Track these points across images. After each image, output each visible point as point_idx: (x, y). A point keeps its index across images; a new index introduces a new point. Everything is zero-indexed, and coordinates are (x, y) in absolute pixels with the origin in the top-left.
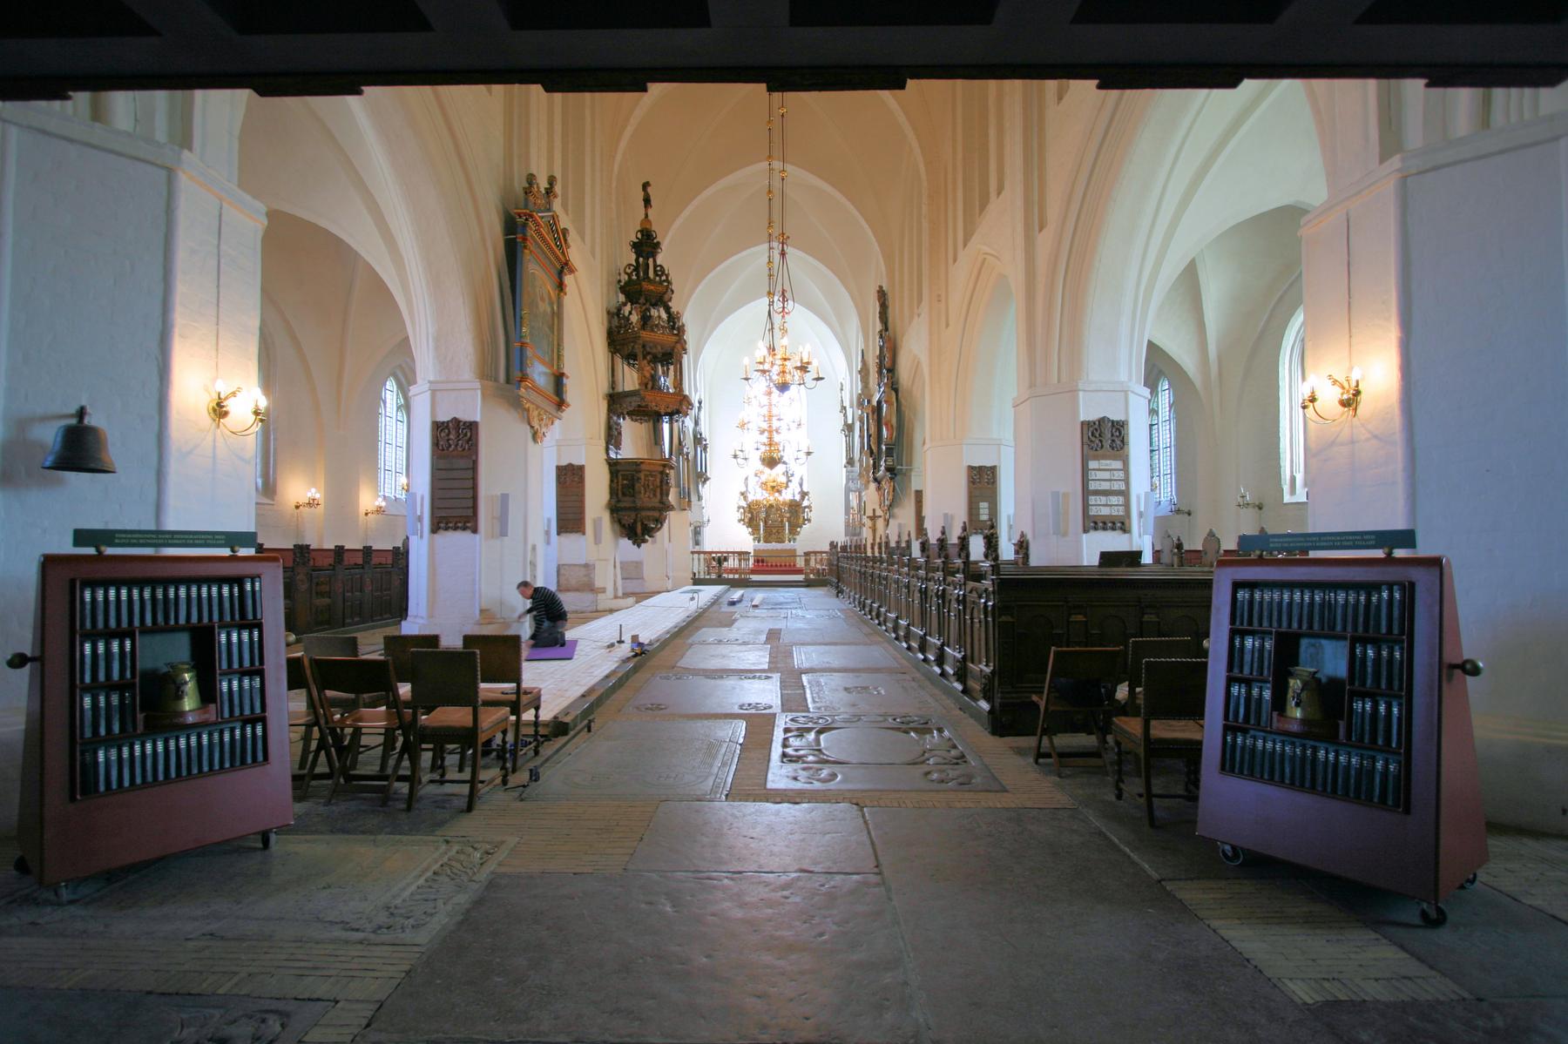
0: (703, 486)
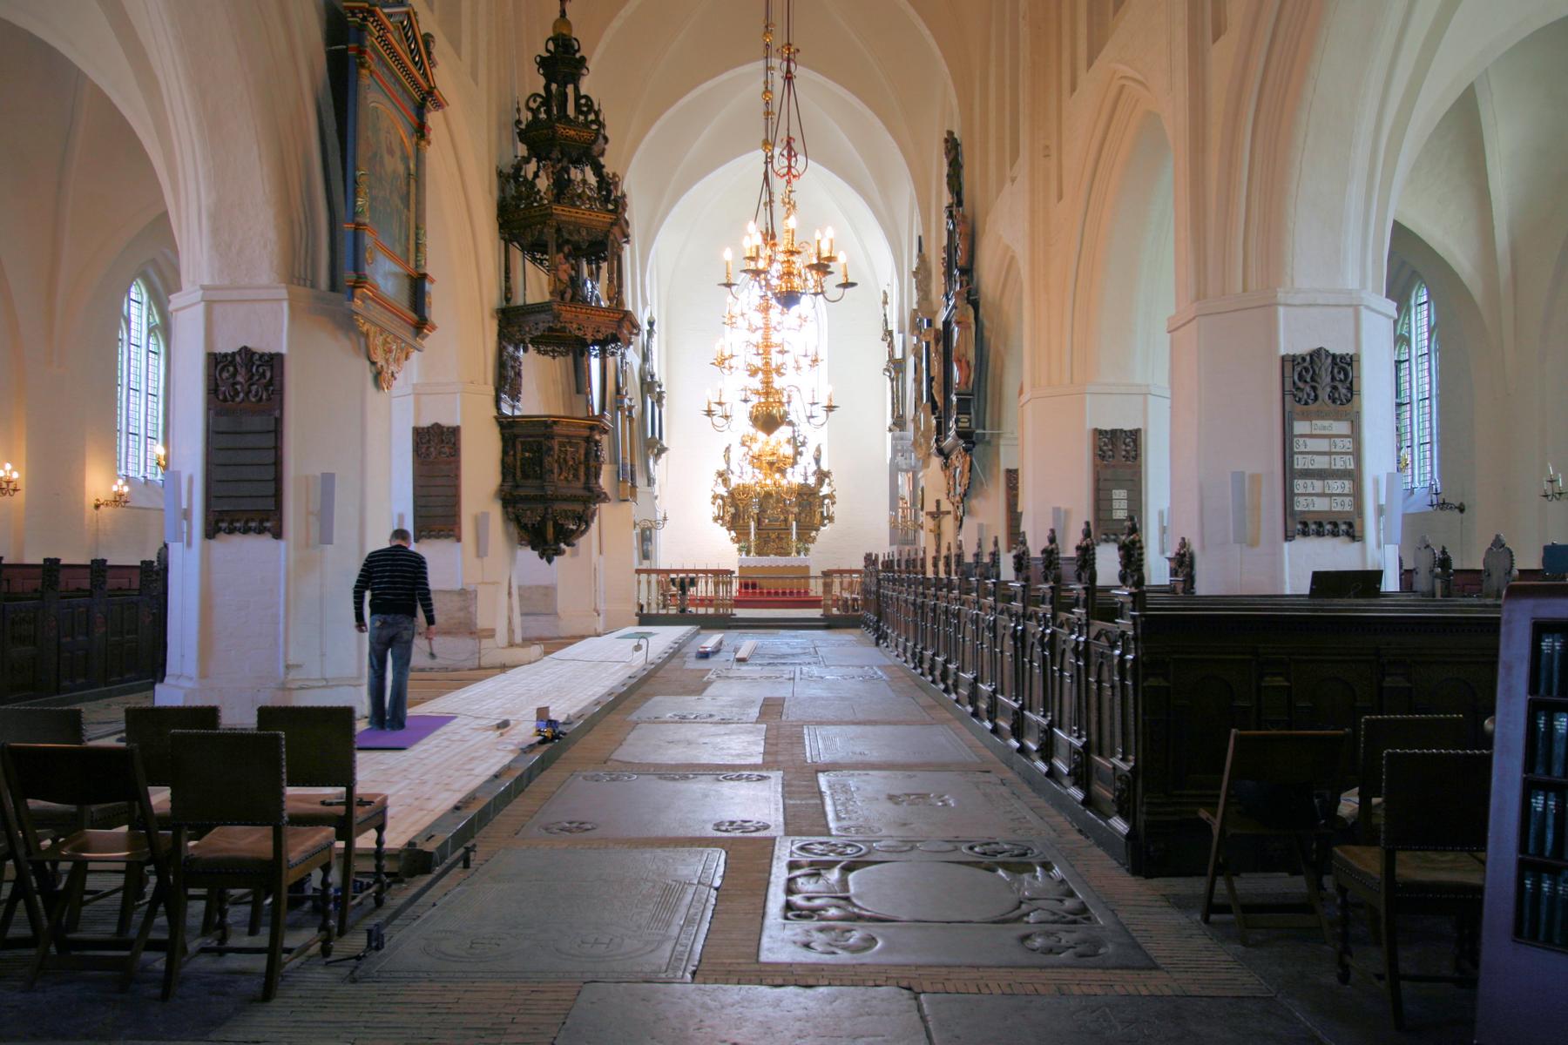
0: (655, 462)
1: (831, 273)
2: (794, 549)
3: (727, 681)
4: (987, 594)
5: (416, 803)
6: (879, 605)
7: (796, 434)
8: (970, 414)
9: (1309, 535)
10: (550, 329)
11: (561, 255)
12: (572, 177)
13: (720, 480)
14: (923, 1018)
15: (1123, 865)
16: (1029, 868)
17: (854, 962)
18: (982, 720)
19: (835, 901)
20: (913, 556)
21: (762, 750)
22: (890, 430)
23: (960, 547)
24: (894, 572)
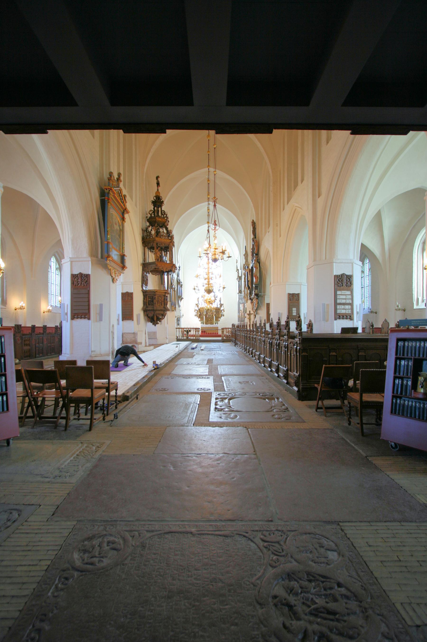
0: (181, 301)
6: (235, 337)
10: (155, 268)
11: (158, 250)
12: (160, 230)
14: (249, 434)
18: (261, 364)
19: (227, 407)
21: (208, 371)
23: (256, 322)
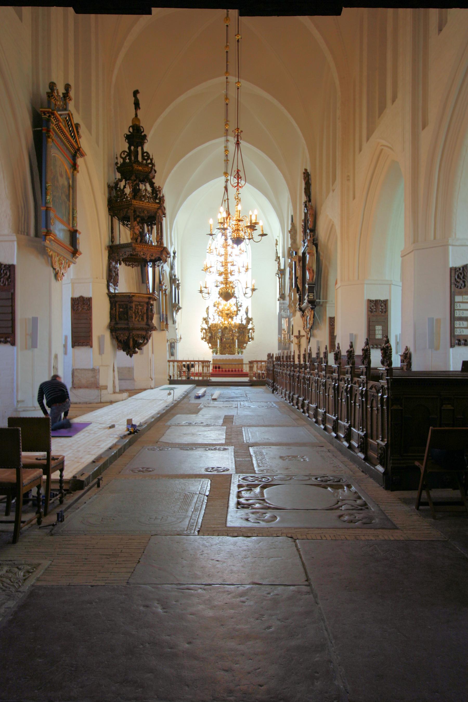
0: (176, 313)
1: (256, 230)
2: (236, 352)
3: (209, 408)
4: (322, 370)
5: (76, 460)
7: (238, 302)
8: (313, 293)
9: (461, 345)
10: (131, 255)
11: (136, 222)
12: (141, 188)
13: (204, 322)
14: (298, 550)
15: (382, 486)
16: (341, 487)
17: (267, 526)
18: (319, 425)
19: (258, 501)
20: (289, 354)
21: (224, 437)
22: (279, 300)
24: (280, 361)
